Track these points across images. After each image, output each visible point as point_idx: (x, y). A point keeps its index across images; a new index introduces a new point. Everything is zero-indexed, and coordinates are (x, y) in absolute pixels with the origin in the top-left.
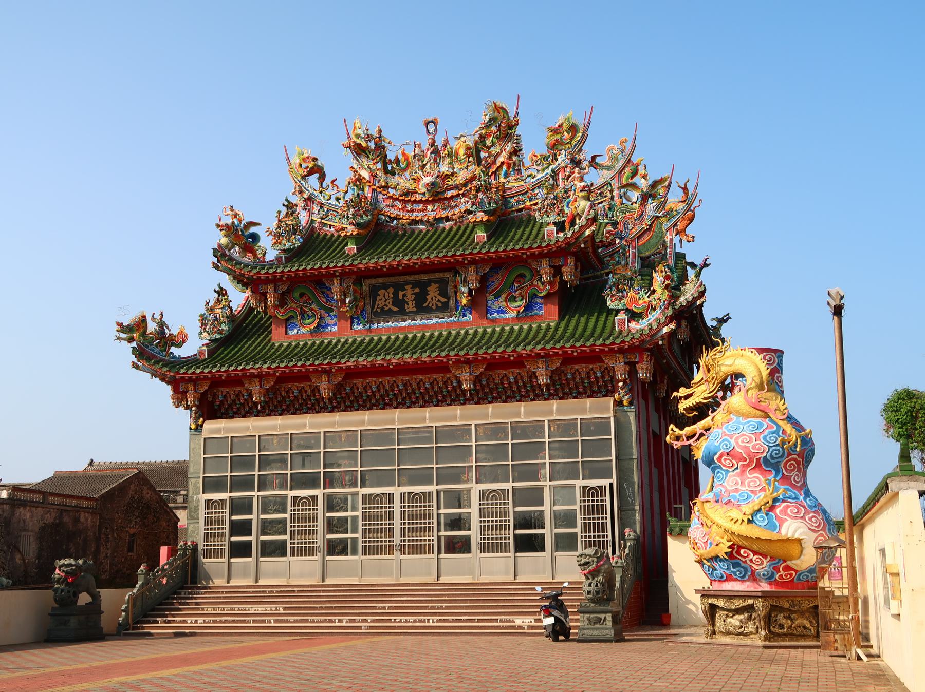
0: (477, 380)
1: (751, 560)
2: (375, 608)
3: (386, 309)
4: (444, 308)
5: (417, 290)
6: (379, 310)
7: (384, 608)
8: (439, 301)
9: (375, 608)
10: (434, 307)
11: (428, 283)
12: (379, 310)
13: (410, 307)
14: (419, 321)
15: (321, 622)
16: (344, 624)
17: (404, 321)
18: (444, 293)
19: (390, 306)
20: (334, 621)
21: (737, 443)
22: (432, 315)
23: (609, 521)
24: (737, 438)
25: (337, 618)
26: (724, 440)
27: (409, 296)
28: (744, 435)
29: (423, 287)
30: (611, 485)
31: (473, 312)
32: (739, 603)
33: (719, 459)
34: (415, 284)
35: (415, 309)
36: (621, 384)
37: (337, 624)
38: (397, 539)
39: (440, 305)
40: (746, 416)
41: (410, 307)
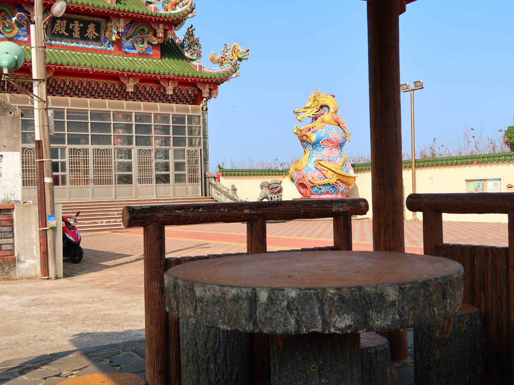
0: (136, 87)
2: (108, 215)
3: (61, 33)
4: (97, 39)
5: (82, 25)
6: (56, 33)
7: (114, 215)
8: (94, 35)
9: (108, 215)
10: (91, 38)
11: (89, 22)
12: (56, 33)
13: (76, 35)
14: (81, 44)
15: (90, 223)
16: (104, 224)
17: (72, 42)
18: (98, 29)
19: (63, 31)
20: (98, 223)
22: (90, 43)
24: (332, 134)
25: (99, 221)
27: (76, 28)
29: (85, 25)
31: (115, 45)
33: (322, 142)
34: (80, 22)
35: (79, 37)
37: (99, 224)
38: (91, 176)
39: (95, 37)
40: (332, 125)
41: (76, 35)
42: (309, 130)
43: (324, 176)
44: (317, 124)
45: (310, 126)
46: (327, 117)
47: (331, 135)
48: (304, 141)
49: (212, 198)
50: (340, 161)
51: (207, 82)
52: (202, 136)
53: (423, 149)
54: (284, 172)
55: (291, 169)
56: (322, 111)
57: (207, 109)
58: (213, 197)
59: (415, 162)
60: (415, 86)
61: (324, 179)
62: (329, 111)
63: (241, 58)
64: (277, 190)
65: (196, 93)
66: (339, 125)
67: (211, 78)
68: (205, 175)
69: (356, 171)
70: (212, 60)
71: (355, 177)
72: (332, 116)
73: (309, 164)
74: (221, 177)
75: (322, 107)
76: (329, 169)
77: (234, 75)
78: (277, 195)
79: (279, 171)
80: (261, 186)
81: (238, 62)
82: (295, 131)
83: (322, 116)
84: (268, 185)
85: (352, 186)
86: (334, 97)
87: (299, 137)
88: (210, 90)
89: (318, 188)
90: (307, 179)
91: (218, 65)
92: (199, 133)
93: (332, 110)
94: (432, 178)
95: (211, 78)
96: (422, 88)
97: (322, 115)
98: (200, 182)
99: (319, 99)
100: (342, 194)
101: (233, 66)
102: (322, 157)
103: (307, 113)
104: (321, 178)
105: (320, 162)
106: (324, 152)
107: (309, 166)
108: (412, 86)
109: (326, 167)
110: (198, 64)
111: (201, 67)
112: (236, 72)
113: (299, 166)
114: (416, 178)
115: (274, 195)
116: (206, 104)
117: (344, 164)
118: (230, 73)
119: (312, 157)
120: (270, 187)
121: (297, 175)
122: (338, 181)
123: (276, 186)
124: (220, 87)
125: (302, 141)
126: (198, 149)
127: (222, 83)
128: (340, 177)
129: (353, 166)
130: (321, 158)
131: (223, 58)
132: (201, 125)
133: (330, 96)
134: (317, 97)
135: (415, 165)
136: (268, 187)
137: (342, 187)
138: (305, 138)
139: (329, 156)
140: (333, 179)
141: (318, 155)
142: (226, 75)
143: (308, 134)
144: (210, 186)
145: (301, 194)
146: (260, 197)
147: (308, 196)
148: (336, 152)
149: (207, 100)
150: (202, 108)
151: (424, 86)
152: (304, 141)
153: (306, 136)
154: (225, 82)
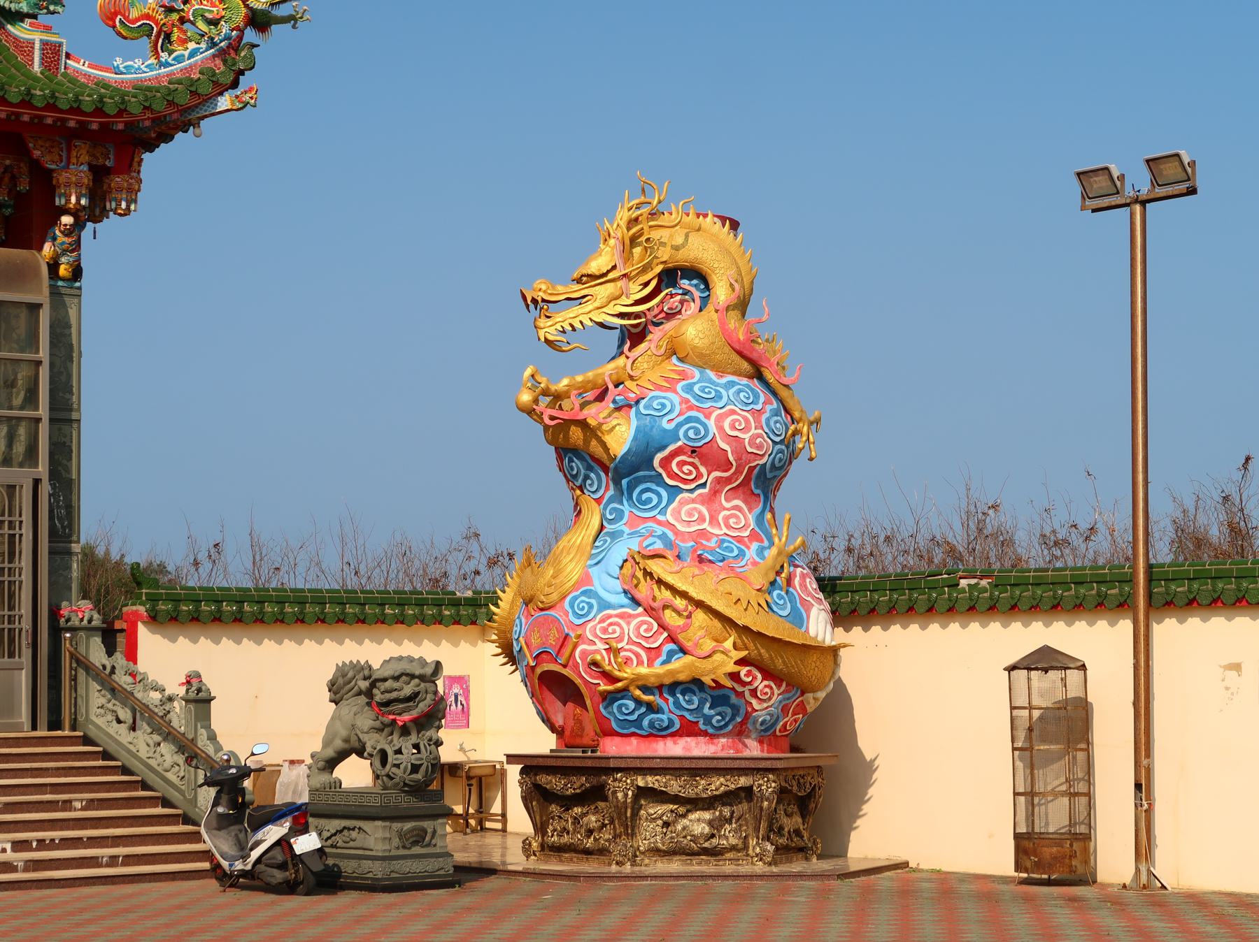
1: (754, 693)
21: (721, 429)
23: (26, 577)
26: (689, 420)
28: (733, 412)
30: (37, 482)
32: (719, 784)
33: (665, 463)
36: (67, 220)
40: (720, 370)
42: (601, 398)
43: (672, 639)
44: (643, 364)
45: (608, 370)
46: (695, 329)
47: (711, 424)
48: (575, 450)
49: (87, 740)
50: (757, 561)
51: (82, 132)
52: (43, 411)
53: (1190, 504)
54: (464, 610)
55: (507, 598)
56: (670, 299)
57: (77, 273)
58: (93, 733)
59: (1150, 579)
60: (1155, 182)
61: (671, 654)
62: (705, 301)
63: (265, 13)
64: (415, 713)
65: (23, 186)
66: (758, 375)
67: (99, 112)
68: (54, 613)
69: (841, 617)
70: (109, 18)
71: (834, 651)
72: (723, 324)
73: (594, 572)
74: (142, 630)
75: (669, 276)
76: (700, 604)
77: (224, 102)
78: (413, 738)
79: (456, 603)
80: (332, 686)
81: (250, 35)
82: (526, 397)
83: (668, 326)
84: (364, 685)
85: (821, 695)
86: (735, 225)
87: (546, 428)
88: (99, 173)
89: (639, 702)
90: (584, 653)
91: (145, 43)
92: (31, 398)
93: (722, 293)
94: (1237, 667)
95: (99, 112)
96: (1192, 191)
97: (670, 316)
98: (27, 653)
99: (655, 235)
100: (768, 735)
101: (222, 54)
102: (663, 537)
103: (589, 307)
104: (653, 653)
105: (656, 567)
106: (683, 513)
107: (597, 587)
108: (1140, 181)
109: (684, 595)
110: (37, 37)
111: (52, 53)
112: (235, 84)
113: (543, 581)
114: (1131, 661)
115: (397, 741)
116: (77, 246)
117: (778, 580)
118: (205, 89)
119: (615, 535)
120: (379, 697)
121: (530, 630)
122: (743, 671)
123: (408, 690)
124: (153, 163)
125: (565, 452)
126: (22, 476)
127: (168, 138)
128: (755, 650)
129: (828, 586)
130: (659, 546)
131: (170, 10)
132: (44, 353)
133: (710, 223)
134: (643, 225)
135: (1149, 595)
136: (369, 693)
137: (766, 701)
138: (576, 434)
139: (703, 534)
140: (720, 658)
141: (642, 528)
142: (183, 99)
143: (594, 414)
144: (82, 675)
145: (553, 729)
146: (327, 743)
147: (586, 741)
148: (737, 515)
149: (79, 225)
150: (53, 267)
151: (1200, 183)
152: (575, 452)
153: (583, 424)
154: (179, 136)
